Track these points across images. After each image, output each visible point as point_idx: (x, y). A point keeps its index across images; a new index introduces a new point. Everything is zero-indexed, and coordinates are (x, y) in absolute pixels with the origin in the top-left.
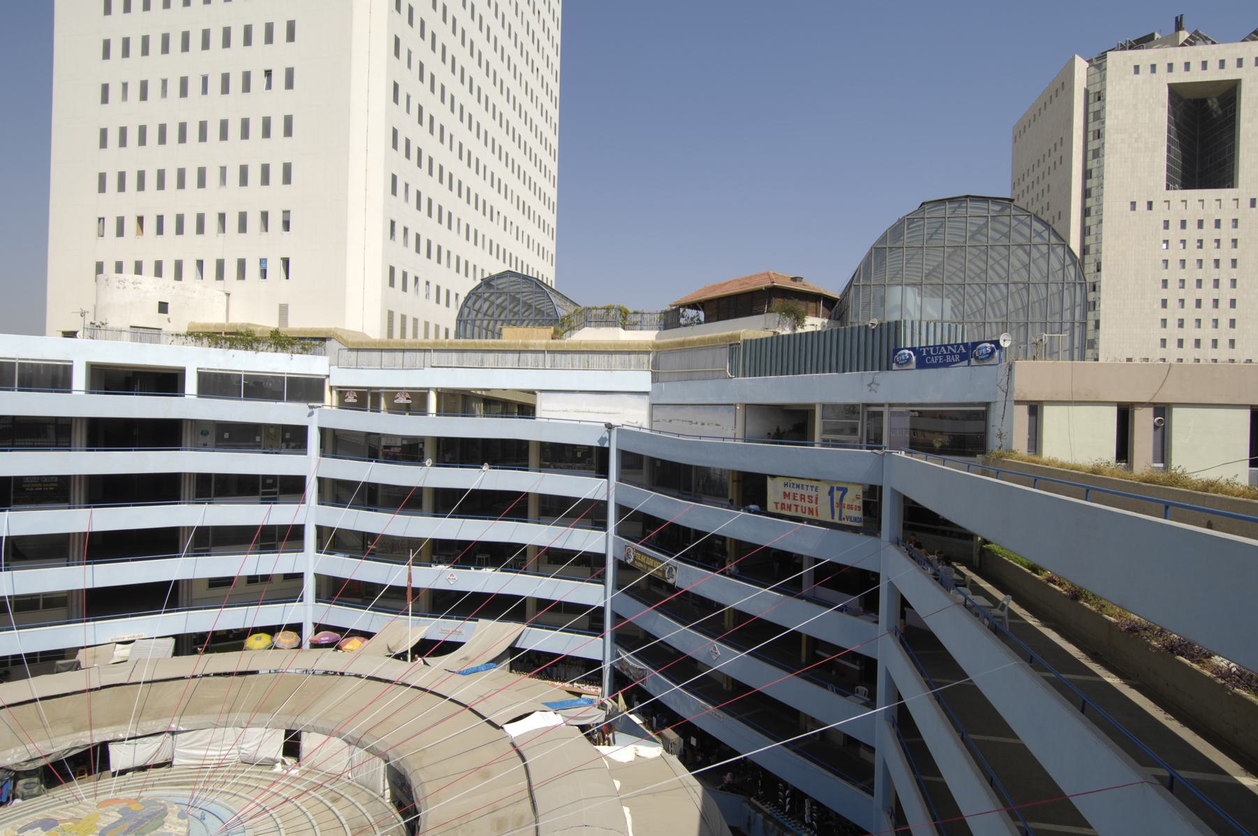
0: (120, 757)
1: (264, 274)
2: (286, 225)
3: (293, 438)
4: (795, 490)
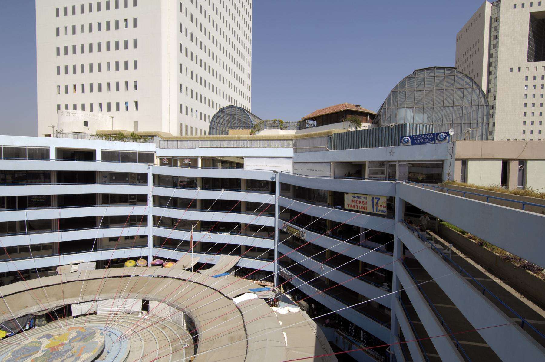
0: (76, 310)
1: (127, 108)
2: (136, 87)
3: (142, 179)
4: (356, 199)
